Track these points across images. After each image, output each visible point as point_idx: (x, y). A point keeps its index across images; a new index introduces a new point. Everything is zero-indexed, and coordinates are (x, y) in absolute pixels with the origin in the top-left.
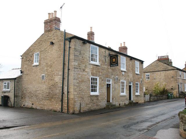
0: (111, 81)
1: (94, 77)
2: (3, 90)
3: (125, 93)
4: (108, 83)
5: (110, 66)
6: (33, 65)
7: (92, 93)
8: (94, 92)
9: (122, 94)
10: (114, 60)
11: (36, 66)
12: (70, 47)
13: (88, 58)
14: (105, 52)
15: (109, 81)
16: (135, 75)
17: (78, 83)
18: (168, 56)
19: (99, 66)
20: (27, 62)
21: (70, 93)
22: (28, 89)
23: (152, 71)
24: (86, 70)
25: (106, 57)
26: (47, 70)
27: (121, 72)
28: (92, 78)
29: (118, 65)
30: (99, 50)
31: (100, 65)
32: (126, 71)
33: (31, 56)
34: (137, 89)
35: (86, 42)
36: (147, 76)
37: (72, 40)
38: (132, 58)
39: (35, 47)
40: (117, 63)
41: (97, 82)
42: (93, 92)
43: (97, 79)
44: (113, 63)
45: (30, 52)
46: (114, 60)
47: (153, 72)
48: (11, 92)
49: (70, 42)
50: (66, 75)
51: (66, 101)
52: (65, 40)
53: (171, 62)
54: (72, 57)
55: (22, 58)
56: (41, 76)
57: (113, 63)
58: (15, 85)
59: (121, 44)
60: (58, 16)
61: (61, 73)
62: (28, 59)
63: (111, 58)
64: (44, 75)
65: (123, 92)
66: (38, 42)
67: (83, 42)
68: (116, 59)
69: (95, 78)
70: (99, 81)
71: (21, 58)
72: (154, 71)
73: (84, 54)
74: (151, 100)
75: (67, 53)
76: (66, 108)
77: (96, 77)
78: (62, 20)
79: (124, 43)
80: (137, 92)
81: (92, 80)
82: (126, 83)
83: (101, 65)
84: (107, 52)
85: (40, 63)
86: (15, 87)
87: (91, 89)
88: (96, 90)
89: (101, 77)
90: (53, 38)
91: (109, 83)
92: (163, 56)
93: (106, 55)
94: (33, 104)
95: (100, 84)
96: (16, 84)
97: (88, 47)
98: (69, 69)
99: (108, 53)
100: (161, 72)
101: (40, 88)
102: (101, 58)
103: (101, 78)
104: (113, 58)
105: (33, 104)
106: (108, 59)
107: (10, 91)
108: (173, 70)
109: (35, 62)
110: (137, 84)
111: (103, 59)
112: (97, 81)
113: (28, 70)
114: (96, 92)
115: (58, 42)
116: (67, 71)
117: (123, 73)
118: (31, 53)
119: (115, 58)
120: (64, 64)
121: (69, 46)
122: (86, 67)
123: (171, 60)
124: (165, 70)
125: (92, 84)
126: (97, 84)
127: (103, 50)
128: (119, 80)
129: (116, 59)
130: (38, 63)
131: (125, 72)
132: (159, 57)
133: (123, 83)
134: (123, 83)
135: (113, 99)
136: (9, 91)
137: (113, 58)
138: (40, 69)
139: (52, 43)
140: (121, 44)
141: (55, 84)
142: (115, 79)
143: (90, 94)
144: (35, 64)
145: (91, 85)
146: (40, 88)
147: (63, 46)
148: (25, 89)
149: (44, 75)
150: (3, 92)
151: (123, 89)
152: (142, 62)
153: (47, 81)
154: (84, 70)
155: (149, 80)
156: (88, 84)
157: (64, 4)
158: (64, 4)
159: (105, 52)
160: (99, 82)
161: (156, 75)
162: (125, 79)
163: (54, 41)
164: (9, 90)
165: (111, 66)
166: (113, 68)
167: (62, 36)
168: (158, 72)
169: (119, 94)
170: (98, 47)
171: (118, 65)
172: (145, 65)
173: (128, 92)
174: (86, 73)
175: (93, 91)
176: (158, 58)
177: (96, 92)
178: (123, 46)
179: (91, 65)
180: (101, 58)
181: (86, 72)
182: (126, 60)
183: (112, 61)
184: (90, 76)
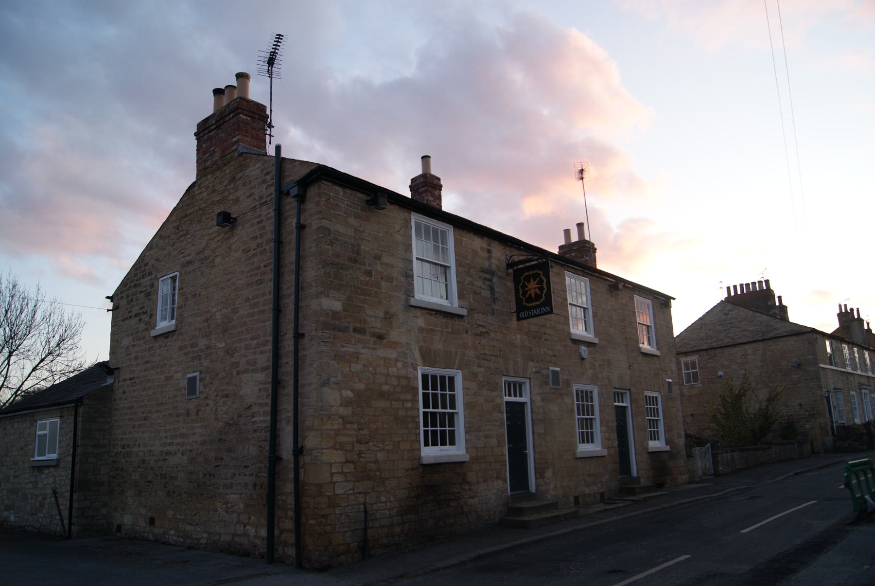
0: (526, 389)
1: (438, 371)
2: (37, 458)
3: (371, 525)
4: (512, 399)
5: (515, 318)
6: (153, 333)
7: (430, 453)
8: (443, 443)
9: (584, 448)
10: (532, 286)
11: (166, 335)
12: (301, 227)
13: (403, 279)
14: (489, 251)
15: (515, 388)
16: (640, 357)
17: (347, 403)
18: (767, 282)
19: (460, 317)
20: (133, 321)
21: (305, 459)
22: (135, 450)
23: (705, 347)
24: (395, 335)
25: (492, 273)
26: (208, 347)
27: (570, 343)
28: (425, 377)
29: (551, 312)
30: (458, 243)
31: (464, 312)
32: (596, 341)
33: (148, 295)
34: (654, 423)
35: (382, 200)
36: (687, 367)
37: (312, 191)
38: (616, 285)
39: (164, 249)
40: (548, 302)
41: (453, 398)
42: (435, 444)
43: (452, 379)
44: (530, 300)
45: (143, 277)
46: (532, 286)
47: (712, 352)
48: (62, 465)
49: (301, 198)
50: (287, 363)
51: (291, 500)
52: (281, 194)
53: (783, 309)
54: (312, 272)
55: (115, 310)
56: (184, 383)
57: (530, 300)
58: (79, 433)
59: (567, 232)
60: (257, 92)
61: (265, 359)
62: (136, 310)
63: (516, 282)
64: (197, 374)
65: (588, 438)
66: (175, 224)
67: (367, 202)
68: (541, 282)
69: (443, 378)
70: (465, 389)
71: (110, 305)
72: (715, 345)
73: (378, 258)
74: (721, 468)
75: (290, 257)
76: (291, 538)
77: (447, 372)
78: (236, 73)
79: (580, 226)
80: (654, 436)
81: (425, 387)
82: (600, 395)
83: (471, 310)
84: (499, 254)
85: (180, 321)
86: (79, 442)
87: (426, 432)
88: (452, 433)
89: (476, 370)
90: (231, 197)
91: (518, 399)
92: (744, 283)
93: (494, 267)
94: (152, 521)
95: (468, 406)
96: (79, 426)
97: (398, 227)
98: (298, 336)
99: (503, 258)
100: (747, 347)
101: (179, 440)
102: (468, 279)
103: (475, 375)
104: (525, 279)
105: (152, 521)
106: (505, 288)
107: (58, 460)
108: (794, 338)
109: (164, 318)
110: (654, 400)
111: (479, 283)
112: (452, 388)
113: (136, 358)
114: (452, 443)
115: (254, 208)
116: (292, 342)
117: (583, 348)
118: (146, 281)
119: (535, 276)
120: (278, 311)
121: (299, 219)
122: (389, 317)
123: (780, 298)
124: (762, 340)
125: (426, 405)
126: (453, 406)
127: (477, 243)
128: (568, 384)
129: (541, 282)
130: (174, 322)
131: (589, 344)
132: (728, 288)
133: (585, 396)
134: (585, 396)
135: (540, 473)
136: (54, 463)
137: (528, 279)
138: (181, 348)
139: (227, 220)
140: (567, 232)
141: (240, 416)
142: (548, 376)
143: (420, 458)
144: (163, 325)
145: (425, 414)
146: (179, 440)
147: (270, 226)
148: (123, 446)
149: (197, 374)
150: (34, 467)
151: (589, 423)
152: (662, 302)
153: (207, 405)
154: (381, 337)
155: (699, 384)
156: (409, 405)
157: (279, 37)
158: (279, 37)
159: (489, 251)
160: (465, 395)
161: (726, 363)
162: (593, 380)
163: (234, 211)
164: (54, 456)
165: (522, 315)
166: (533, 324)
167: (268, 177)
168: (735, 350)
169: (572, 448)
170: (450, 230)
171: (551, 312)
172: (679, 325)
173: (780, 339)
174: (392, 354)
175: (433, 439)
176: (726, 295)
177: (452, 443)
178: (575, 238)
179: (418, 313)
180: (468, 279)
181: (393, 345)
182: (591, 289)
183: (524, 293)
184: (416, 369)
